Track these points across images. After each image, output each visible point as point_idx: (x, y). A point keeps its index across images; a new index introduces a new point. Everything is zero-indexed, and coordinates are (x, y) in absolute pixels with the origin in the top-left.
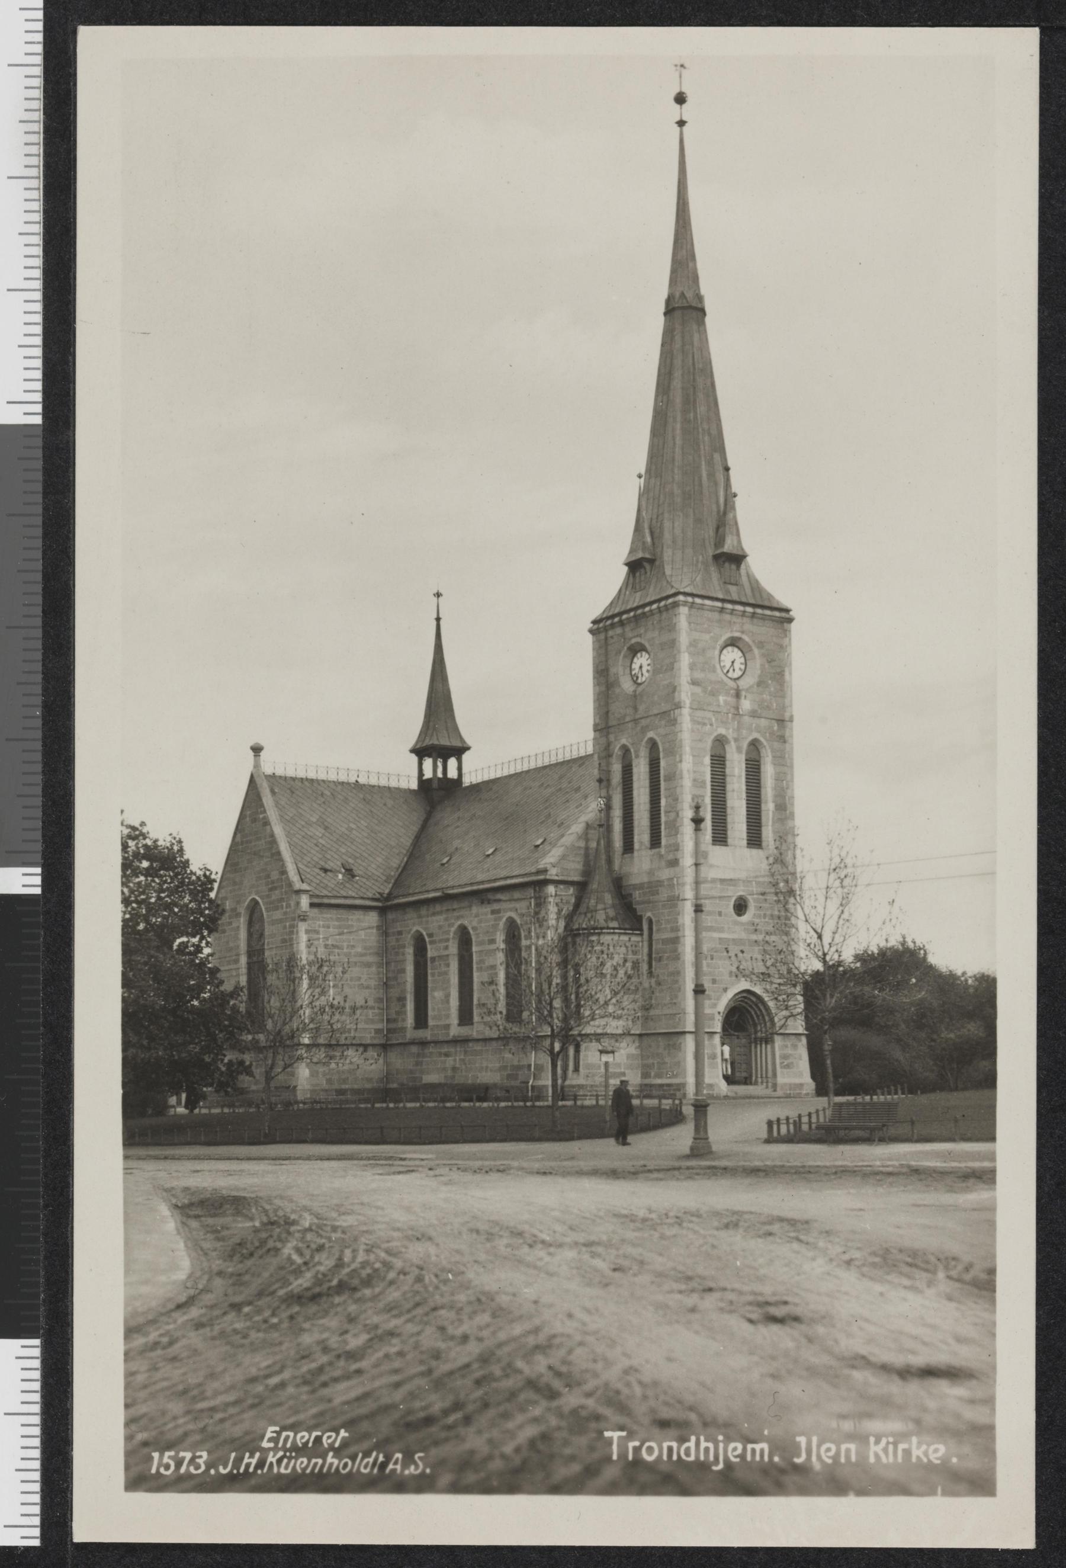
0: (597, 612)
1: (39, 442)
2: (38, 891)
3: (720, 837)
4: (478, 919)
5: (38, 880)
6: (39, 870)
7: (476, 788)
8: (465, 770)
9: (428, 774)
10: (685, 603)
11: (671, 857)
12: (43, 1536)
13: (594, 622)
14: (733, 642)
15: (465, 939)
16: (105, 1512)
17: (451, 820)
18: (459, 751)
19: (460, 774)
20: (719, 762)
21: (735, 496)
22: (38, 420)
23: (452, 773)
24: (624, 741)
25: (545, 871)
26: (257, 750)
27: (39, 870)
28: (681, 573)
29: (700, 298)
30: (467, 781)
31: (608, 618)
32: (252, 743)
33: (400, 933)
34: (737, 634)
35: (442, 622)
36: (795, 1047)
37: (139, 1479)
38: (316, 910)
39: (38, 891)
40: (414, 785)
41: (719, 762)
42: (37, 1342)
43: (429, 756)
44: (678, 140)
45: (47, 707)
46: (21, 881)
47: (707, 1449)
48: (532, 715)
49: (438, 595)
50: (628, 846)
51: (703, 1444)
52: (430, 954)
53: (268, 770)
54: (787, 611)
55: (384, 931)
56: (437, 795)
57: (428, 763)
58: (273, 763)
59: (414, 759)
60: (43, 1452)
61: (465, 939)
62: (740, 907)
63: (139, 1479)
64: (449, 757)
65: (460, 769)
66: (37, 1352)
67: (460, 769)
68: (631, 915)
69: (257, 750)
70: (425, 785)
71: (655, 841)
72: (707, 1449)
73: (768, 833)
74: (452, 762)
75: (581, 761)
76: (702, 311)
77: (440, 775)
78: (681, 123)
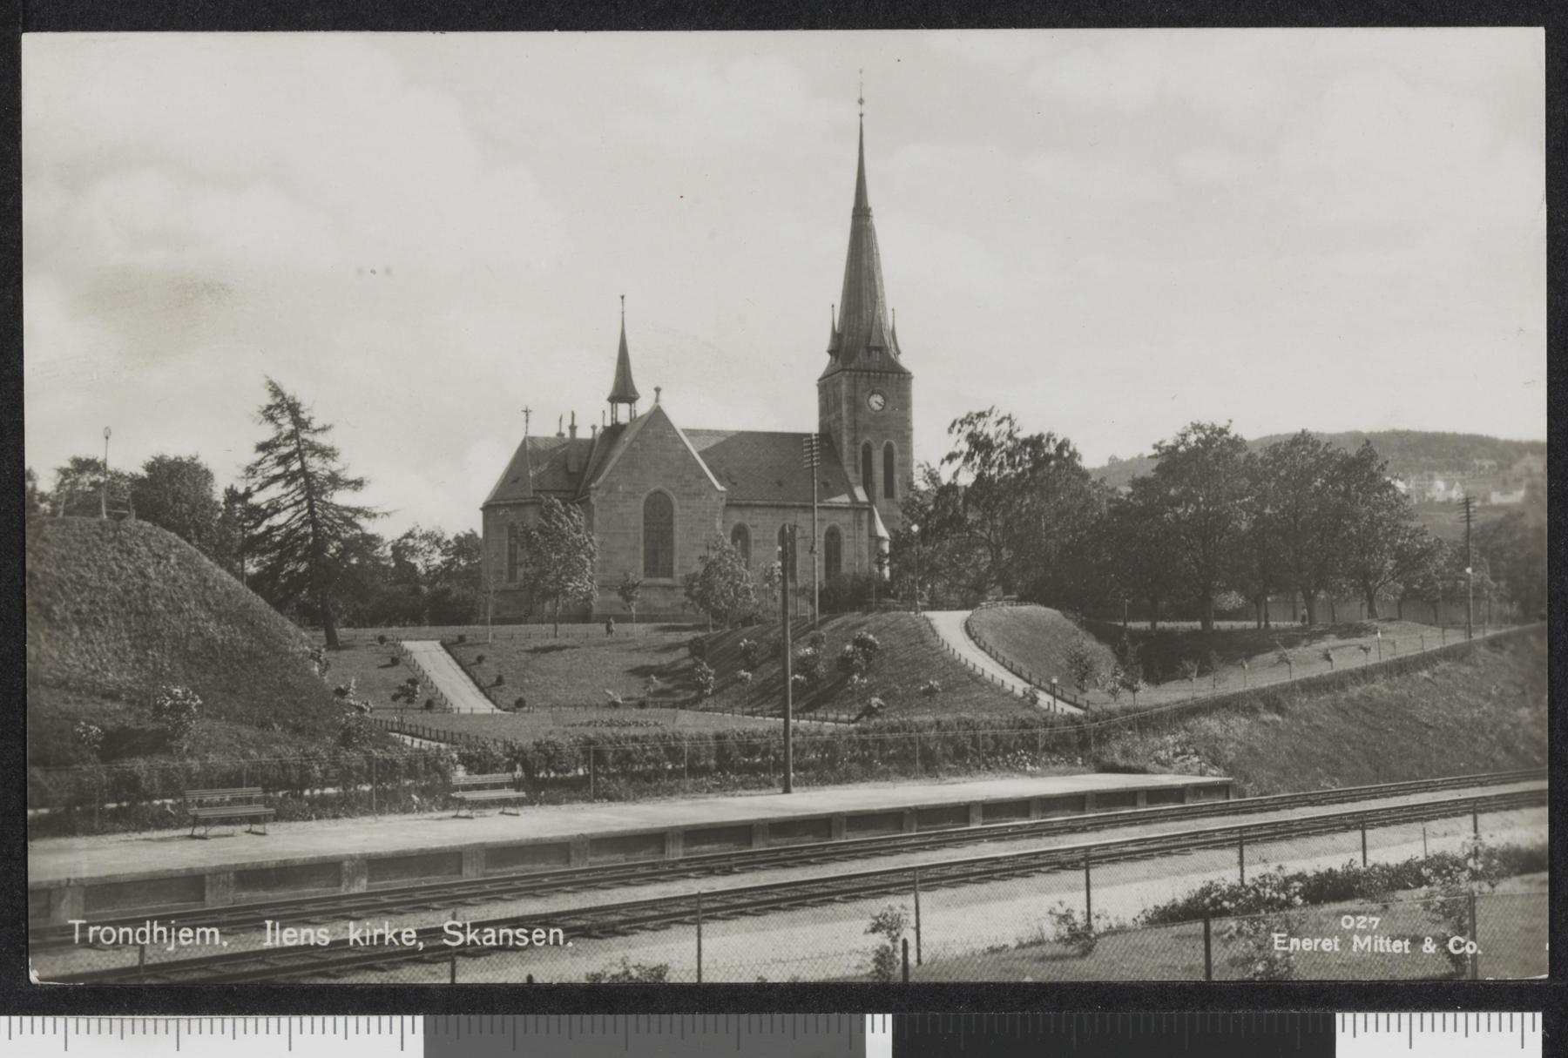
1: (442, 1018)
2: (889, 1017)
5: (878, 1017)
6: (868, 1017)
12: (1533, 1009)
22: (420, 1019)
39: (889, 1017)
42: (1339, 1016)
46: (879, 1034)
47: (160, 933)
51: (156, 930)
66: (1349, 1016)
72: (160, 933)
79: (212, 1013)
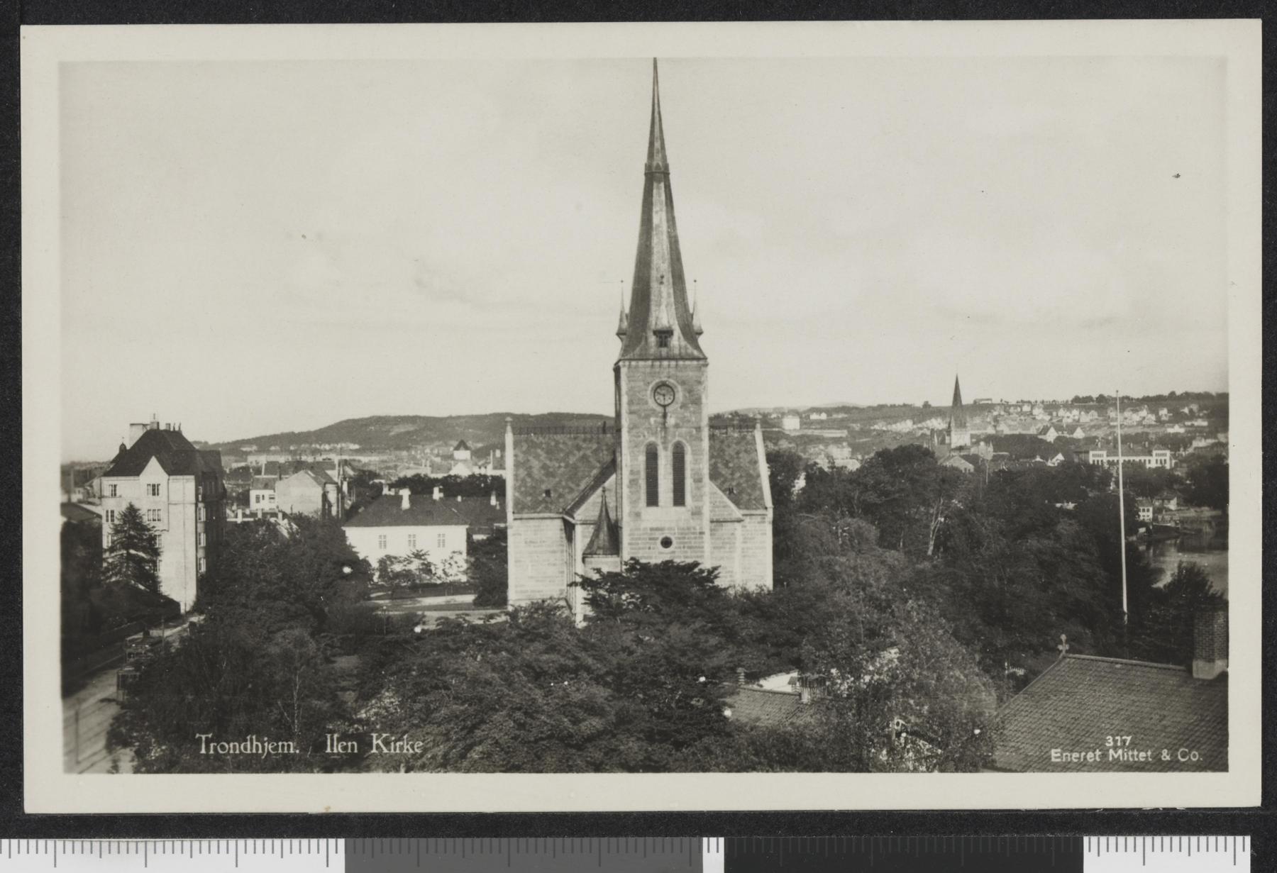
1: (359, 841)
2: (722, 840)
5: (713, 840)
6: (705, 840)
12: (1243, 833)
16: (1240, 783)
20: (652, 457)
22: (342, 842)
27: (705, 840)
37: (1216, 760)
39: (722, 840)
41: (652, 457)
42: (1086, 839)
45: (383, 834)
46: (713, 853)
60: (1193, 834)
63: (1216, 760)
66: (1094, 839)
79: (173, 837)
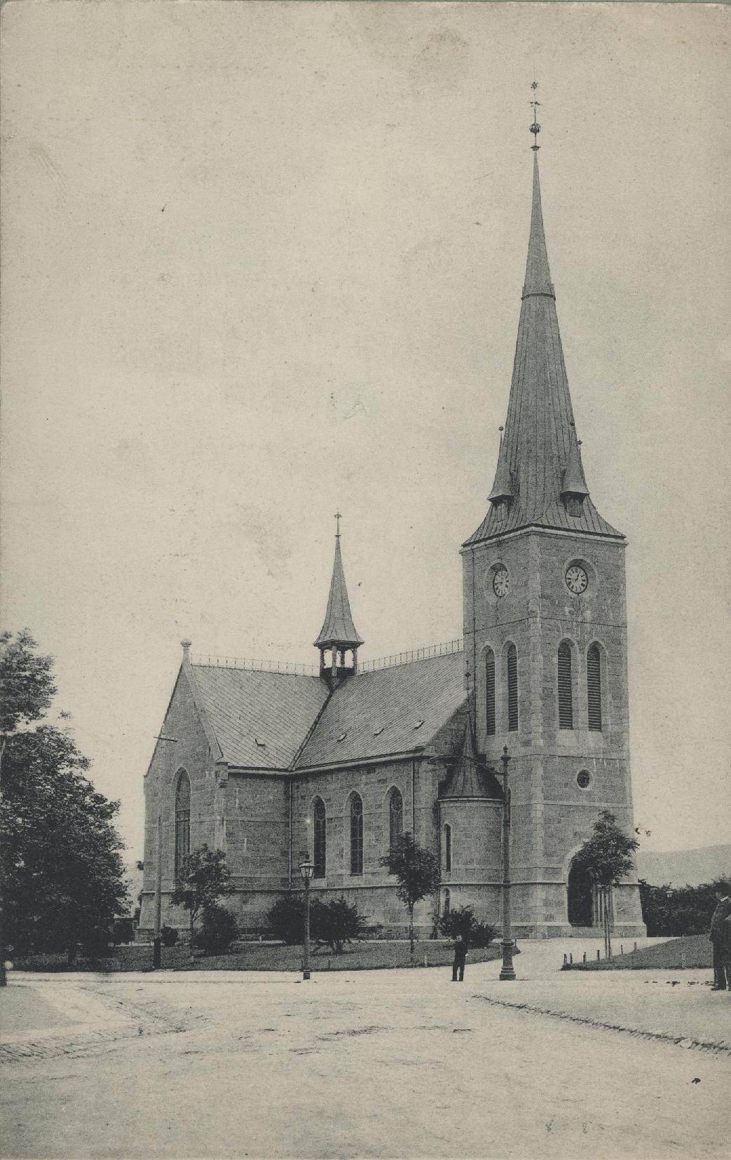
0: (466, 536)
3: (567, 721)
4: (366, 786)
7: (366, 674)
8: (359, 662)
9: (329, 664)
10: (536, 533)
11: (526, 738)
13: (464, 545)
14: (577, 564)
15: (356, 803)
17: (347, 698)
18: (354, 646)
19: (355, 665)
21: (580, 443)
23: (349, 663)
24: (487, 643)
25: (422, 749)
26: (186, 645)
28: (533, 502)
29: (551, 287)
30: (360, 669)
31: (475, 542)
32: (182, 639)
33: (303, 798)
34: (581, 557)
35: (341, 539)
36: (630, 895)
38: (232, 779)
40: (317, 673)
43: (330, 648)
44: (529, 202)
48: (415, 615)
49: (338, 516)
50: (491, 730)
52: (327, 816)
53: (195, 661)
54: (623, 537)
55: (289, 797)
56: (335, 679)
57: (328, 655)
58: (199, 655)
59: (318, 651)
61: (356, 803)
62: (584, 779)
64: (347, 649)
65: (355, 659)
67: (355, 659)
68: (494, 788)
69: (186, 645)
70: (325, 673)
71: (513, 726)
73: (607, 719)
74: (349, 654)
75: (453, 656)
76: (553, 297)
77: (338, 665)
78: (535, 130)
